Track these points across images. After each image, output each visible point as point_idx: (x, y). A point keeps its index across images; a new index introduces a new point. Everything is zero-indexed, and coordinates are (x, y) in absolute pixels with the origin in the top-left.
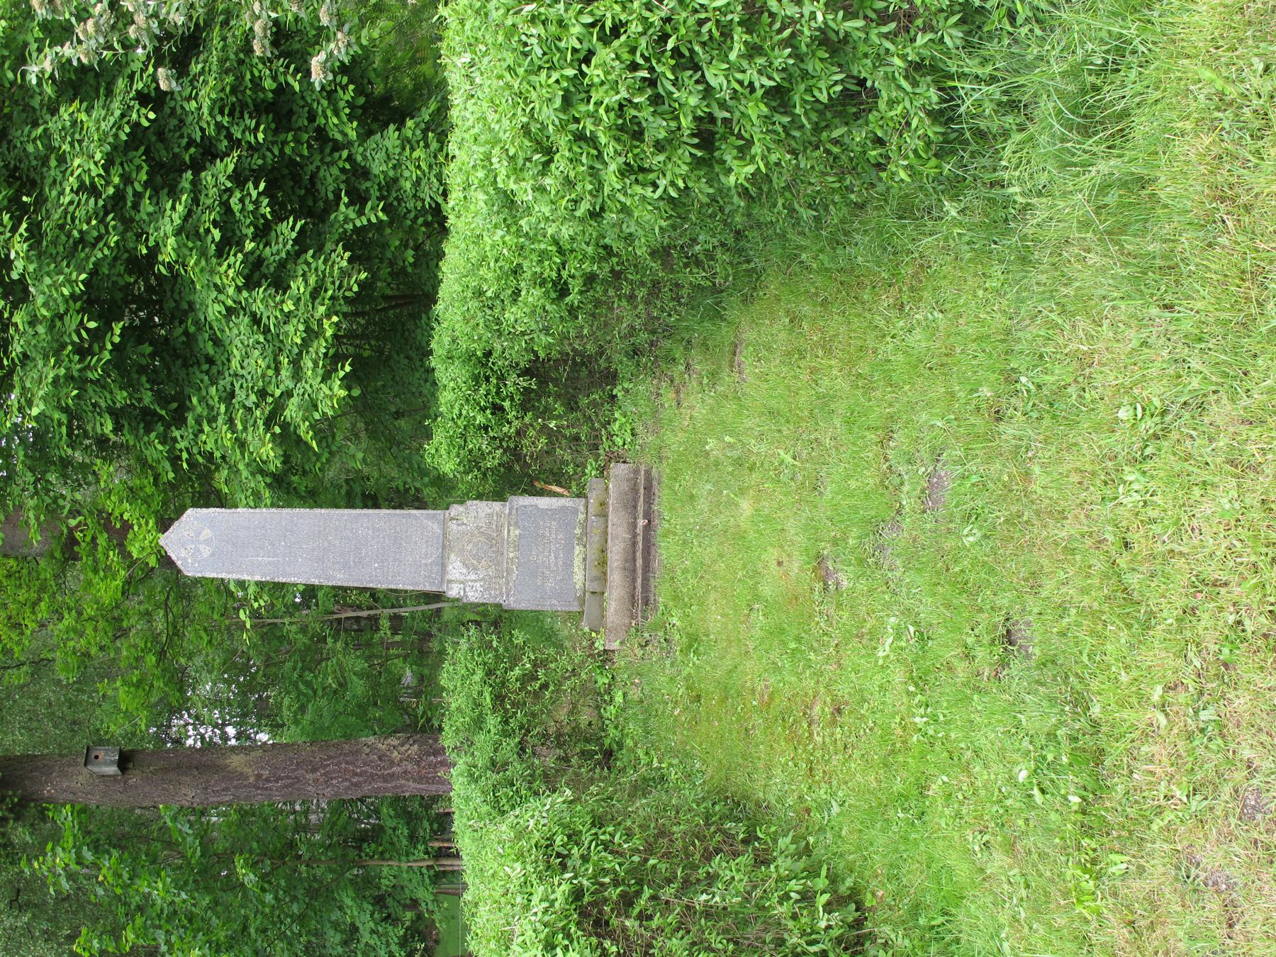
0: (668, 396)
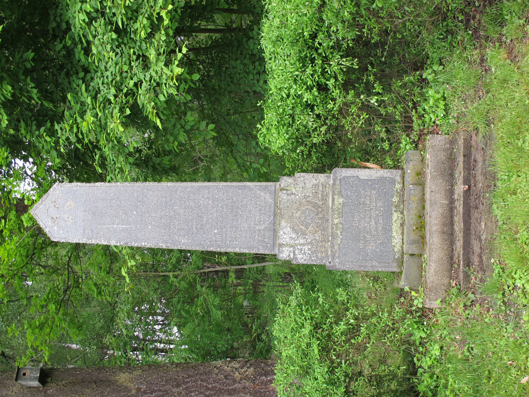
0: (496, 57)
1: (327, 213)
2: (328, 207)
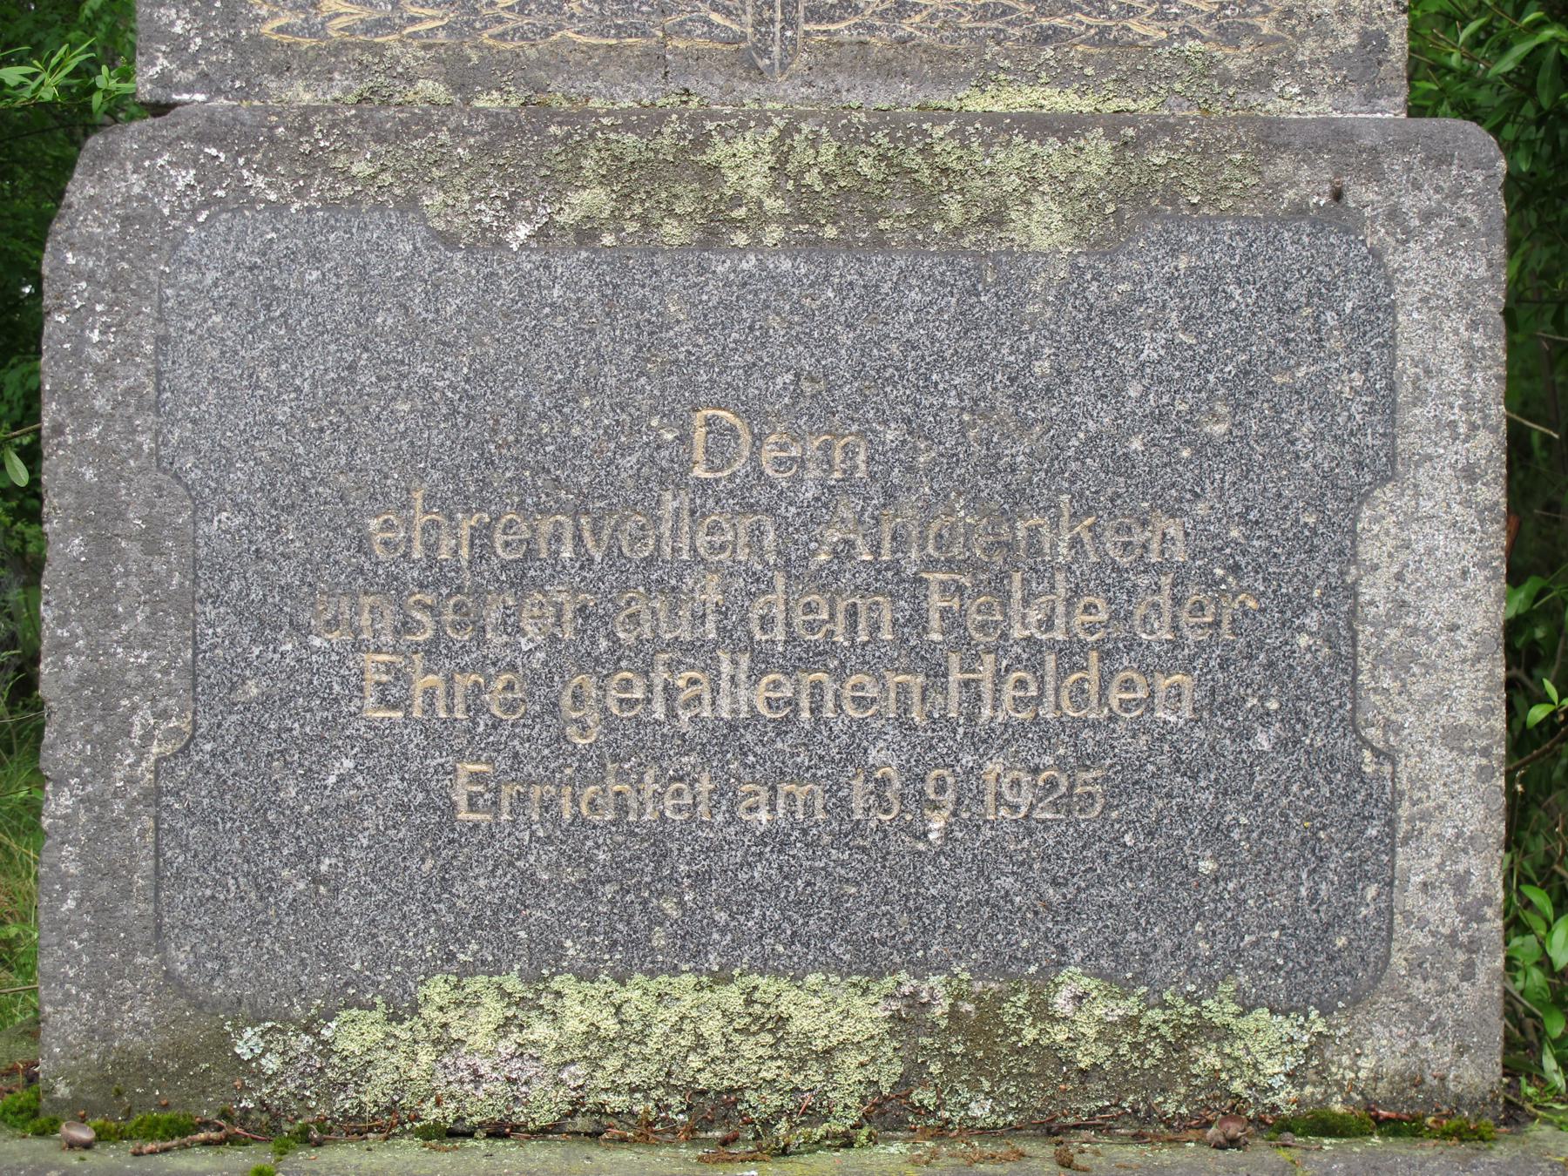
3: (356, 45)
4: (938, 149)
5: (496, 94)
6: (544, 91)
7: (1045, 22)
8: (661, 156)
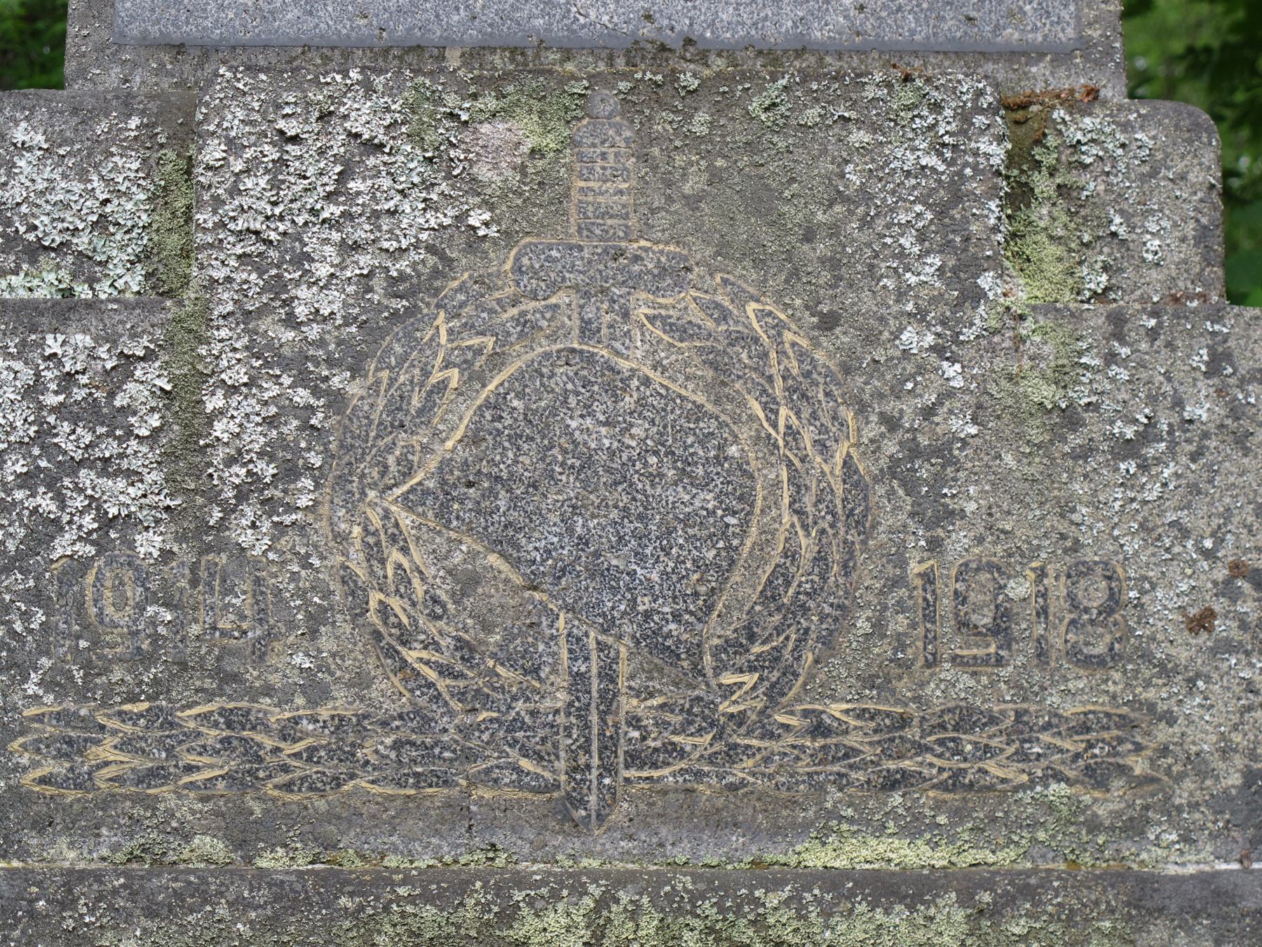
1: (685, 810)
2: (782, 814)
3: (126, 797)
4: (771, 920)
5: (280, 851)
6: (334, 847)
7: (892, 765)
8: (463, 931)
